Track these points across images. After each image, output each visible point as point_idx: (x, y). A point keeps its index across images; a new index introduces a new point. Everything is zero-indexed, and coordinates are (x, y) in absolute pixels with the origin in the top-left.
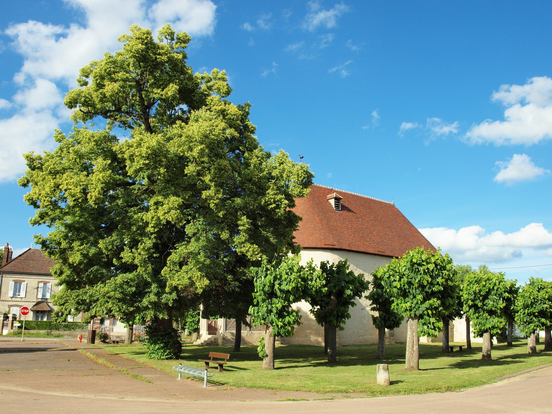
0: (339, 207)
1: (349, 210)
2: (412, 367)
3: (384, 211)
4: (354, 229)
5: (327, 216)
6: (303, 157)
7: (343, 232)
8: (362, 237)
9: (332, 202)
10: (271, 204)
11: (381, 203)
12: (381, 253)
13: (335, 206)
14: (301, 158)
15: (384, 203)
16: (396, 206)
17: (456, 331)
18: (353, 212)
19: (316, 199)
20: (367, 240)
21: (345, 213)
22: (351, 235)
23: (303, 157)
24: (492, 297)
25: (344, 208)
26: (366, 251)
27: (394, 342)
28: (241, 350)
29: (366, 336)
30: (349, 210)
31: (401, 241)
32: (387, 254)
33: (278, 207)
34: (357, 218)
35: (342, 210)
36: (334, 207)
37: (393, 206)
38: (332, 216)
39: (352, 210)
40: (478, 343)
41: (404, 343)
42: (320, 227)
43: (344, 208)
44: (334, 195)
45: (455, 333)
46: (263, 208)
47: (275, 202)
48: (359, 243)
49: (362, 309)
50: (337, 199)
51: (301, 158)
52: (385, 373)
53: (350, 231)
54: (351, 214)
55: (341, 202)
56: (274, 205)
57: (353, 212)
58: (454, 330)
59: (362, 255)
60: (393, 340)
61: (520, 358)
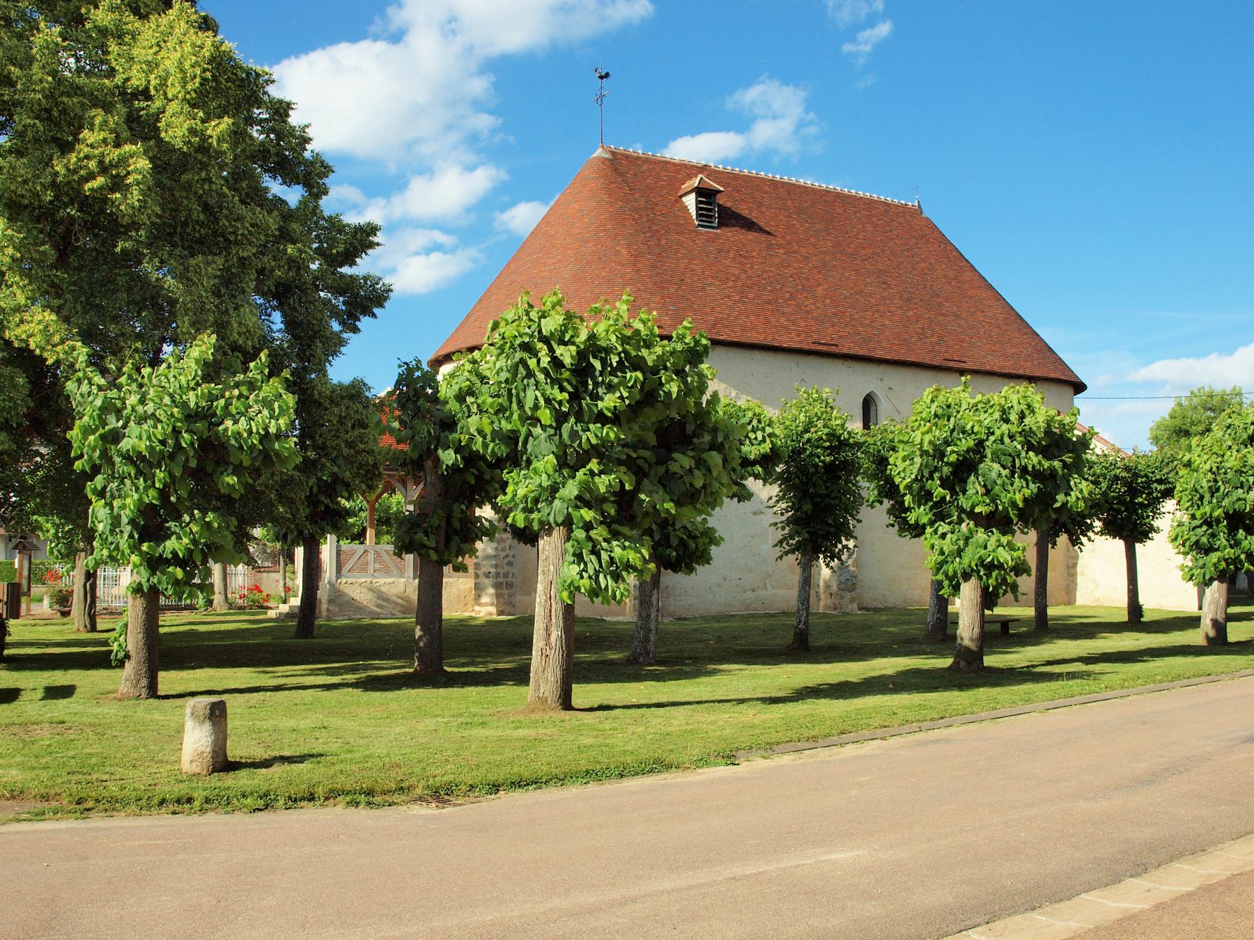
0: (711, 217)
1: (750, 225)
2: (543, 700)
3: (875, 226)
4: (749, 278)
5: (663, 242)
6: (607, 75)
7: (703, 289)
8: (769, 303)
9: (690, 201)
10: (91, 176)
11: (870, 203)
12: (825, 348)
13: (699, 215)
14: (601, 77)
15: (885, 204)
16: (927, 213)
17: (1083, 574)
18: (761, 230)
19: (637, 196)
20: (786, 310)
21: (732, 234)
22: (728, 297)
23: (607, 75)
24: (992, 469)
25: (729, 218)
26: (769, 341)
27: (855, 606)
28: (315, 632)
29: (766, 588)
30: (750, 225)
31: (911, 313)
32: (845, 351)
33: (118, 184)
34: (769, 247)
35: (720, 225)
36: (694, 217)
37: (911, 216)
38: (681, 244)
39: (761, 224)
40: (1171, 612)
41: (530, 621)
42: (629, 276)
43: (729, 218)
44: (695, 182)
45: (1080, 579)
46: (69, 191)
47: (104, 169)
48: (752, 318)
49: (755, 514)
50: (704, 194)
51: (601, 77)
52: (197, 730)
53: (731, 284)
54: (752, 236)
55: (721, 200)
56: (100, 181)
57: (761, 230)
58: (1079, 569)
59: (758, 356)
60: (852, 601)
61: (917, 672)
